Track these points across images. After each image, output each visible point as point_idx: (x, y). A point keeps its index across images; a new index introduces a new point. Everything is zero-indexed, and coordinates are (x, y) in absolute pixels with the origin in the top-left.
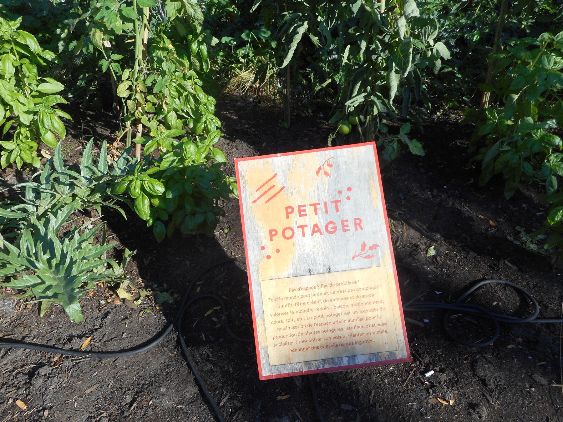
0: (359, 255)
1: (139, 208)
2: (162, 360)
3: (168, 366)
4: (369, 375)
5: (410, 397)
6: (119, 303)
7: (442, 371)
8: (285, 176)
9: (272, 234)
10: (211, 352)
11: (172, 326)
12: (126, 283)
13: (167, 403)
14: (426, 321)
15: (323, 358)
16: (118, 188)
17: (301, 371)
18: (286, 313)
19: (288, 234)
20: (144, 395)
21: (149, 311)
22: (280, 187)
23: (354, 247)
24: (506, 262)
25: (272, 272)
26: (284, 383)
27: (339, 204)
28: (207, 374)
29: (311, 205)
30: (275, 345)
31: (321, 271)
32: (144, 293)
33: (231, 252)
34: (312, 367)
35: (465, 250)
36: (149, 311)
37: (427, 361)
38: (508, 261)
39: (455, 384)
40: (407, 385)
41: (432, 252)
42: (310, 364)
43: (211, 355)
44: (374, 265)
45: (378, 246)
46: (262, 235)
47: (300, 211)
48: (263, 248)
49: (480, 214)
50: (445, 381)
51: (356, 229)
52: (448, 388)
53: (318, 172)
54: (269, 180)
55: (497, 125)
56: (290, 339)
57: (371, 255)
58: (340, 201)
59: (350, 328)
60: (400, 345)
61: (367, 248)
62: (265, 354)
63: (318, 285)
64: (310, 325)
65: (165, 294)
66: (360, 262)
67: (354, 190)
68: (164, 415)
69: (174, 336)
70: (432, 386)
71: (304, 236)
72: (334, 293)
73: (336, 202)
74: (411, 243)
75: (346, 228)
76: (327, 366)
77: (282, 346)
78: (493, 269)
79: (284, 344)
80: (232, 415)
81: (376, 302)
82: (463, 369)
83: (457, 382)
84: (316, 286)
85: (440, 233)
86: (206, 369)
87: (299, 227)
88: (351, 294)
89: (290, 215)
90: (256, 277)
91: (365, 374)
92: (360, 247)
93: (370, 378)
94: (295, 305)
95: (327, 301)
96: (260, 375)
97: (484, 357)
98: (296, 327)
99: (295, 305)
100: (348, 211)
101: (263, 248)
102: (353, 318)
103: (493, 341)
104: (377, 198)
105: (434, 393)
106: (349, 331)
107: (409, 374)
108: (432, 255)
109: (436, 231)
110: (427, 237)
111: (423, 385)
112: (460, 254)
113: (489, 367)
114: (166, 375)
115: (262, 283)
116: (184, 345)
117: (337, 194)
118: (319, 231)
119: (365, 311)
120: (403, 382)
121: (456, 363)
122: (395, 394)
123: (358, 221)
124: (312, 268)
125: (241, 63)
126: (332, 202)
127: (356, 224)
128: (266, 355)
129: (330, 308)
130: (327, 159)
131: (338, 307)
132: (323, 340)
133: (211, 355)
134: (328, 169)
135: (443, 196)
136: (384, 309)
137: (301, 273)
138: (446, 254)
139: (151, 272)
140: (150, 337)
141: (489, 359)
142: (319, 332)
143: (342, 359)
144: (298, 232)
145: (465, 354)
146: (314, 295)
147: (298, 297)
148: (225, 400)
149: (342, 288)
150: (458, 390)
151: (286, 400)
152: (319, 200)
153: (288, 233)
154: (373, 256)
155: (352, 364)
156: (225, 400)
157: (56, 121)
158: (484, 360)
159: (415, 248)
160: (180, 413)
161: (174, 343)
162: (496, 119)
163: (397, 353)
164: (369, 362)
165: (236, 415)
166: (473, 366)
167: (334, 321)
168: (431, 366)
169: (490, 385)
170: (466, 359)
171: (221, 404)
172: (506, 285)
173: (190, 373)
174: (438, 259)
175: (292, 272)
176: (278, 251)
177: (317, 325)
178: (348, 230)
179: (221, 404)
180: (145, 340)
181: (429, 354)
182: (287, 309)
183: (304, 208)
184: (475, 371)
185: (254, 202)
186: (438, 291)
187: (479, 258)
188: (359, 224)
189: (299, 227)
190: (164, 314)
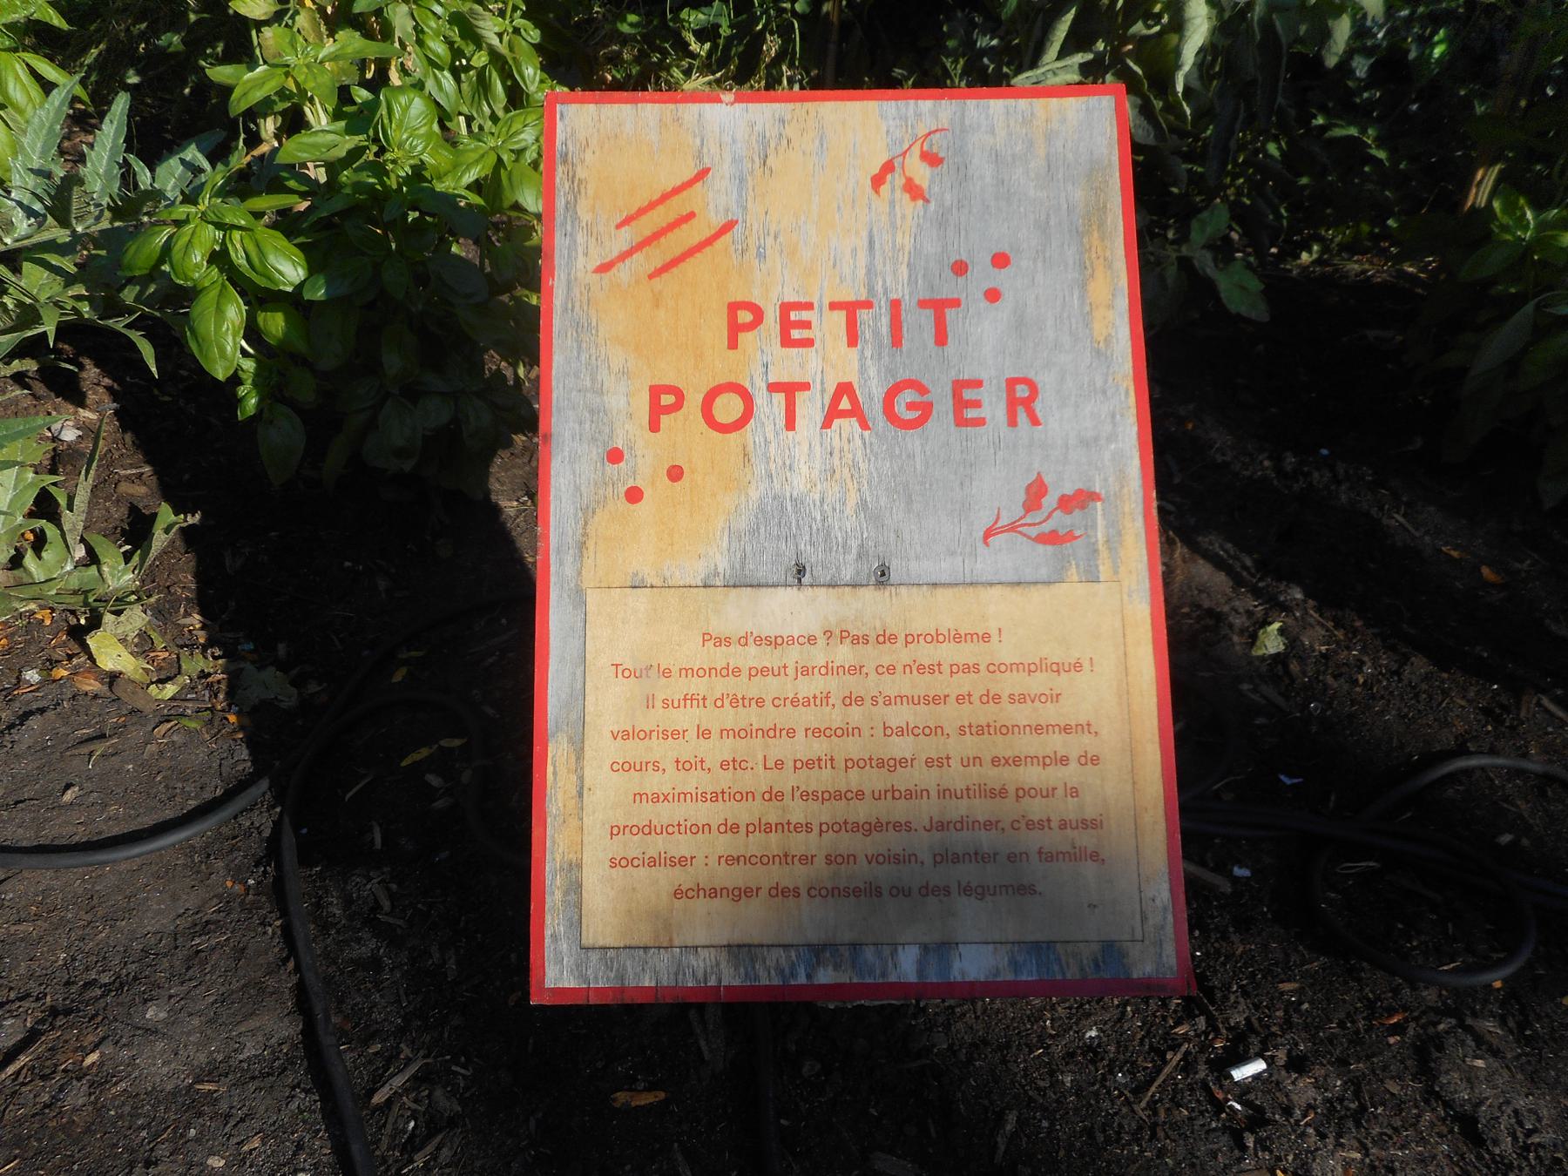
0: (1012, 528)
1: (201, 330)
2: (190, 901)
3: (205, 928)
4: (1000, 1048)
5: (1161, 1153)
6: (91, 685)
7: (1297, 1064)
8: (742, 180)
9: (662, 403)
10: (392, 896)
11: (264, 784)
12: (136, 619)
13: (159, 1066)
14: (1240, 872)
15: (813, 937)
16: (133, 248)
17: (712, 982)
18: (676, 734)
19: (727, 409)
20: (72, 1027)
21: (193, 725)
22: (717, 221)
23: (997, 492)
24: (1545, 701)
25: (641, 560)
26: (630, 1029)
27: (950, 314)
28: (353, 973)
29: (834, 306)
30: (614, 864)
31: (847, 574)
32: (195, 664)
33: (516, 527)
34: (762, 973)
35: (1393, 648)
36: (193, 725)
37: (1238, 1018)
38: (1557, 701)
39: (1350, 1124)
40: (1152, 1105)
41: (1271, 642)
42: (753, 960)
43: (386, 905)
44: (1073, 573)
45: (1095, 497)
46: (616, 401)
47: (786, 325)
48: (615, 456)
49: (1446, 544)
50: (1310, 1107)
51: (1012, 422)
52: (1323, 1136)
53: (877, 181)
54: (677, 191)
55: (1529, 249)
56: (682, 845)
57: (1062, 532)
58: (956, 303)
59: (942, 826)
60: (1153, 920)
61: (1050, 501)
62: (566, 893)
63: (828, 633)
64: (774, 796)
65: (271, 674)
66: (1010, 555)
67: (1021, 263)
68: (134, 1115)
69: (264, 821)
70: (1257, 1119)
71: (790, 424)
72: (891, 669)
73: (939, 307)
74: (1199, 607)
75: (971, 413)
76: (825, 976)
77: (643, 872)
78: (1498, 721)
79: (653, 862)
80: (411, 1146)
81: (1066, 729)
82: (1385, 1068)
83: (1359, 1116)
84: (819, 634)
85: (1301, 584)
86: (354, 955)
87: (773, 388)
88: (963, 683)
89: (743, 337)
90: (569, 571)
91: (985, 1042)
92: (1021, 497)
93: (1004, 1061)
94: (719, 703)
95: (860, 700)
96: (533, 981)
97: (1469, 1030)
98: (715, 797)
99: (719, 703)
100: (984, 344)
101: (615, 456)
102: (960, 785)
103: (1508, 971)
104: (1111, 306)
105: (1265, 1149)
106: (937, 835)
107: (1165, 1062)
108: (1272, 651)
109: (1293, 577)
110: (1256, 593)
111: (1217, 1113)
112: (1375, 660)
113: (1490, 1076)
114: (189, 959)
115: (592, 598)
116: (289, 856)
117: (948, 273)
118: (856, 412)
119: (1016, 761)
120: (1139, 1090)
121: (1356, 1040)
122: (1100, 1138)
123: (1022, 391)
124: (811, 556)
125: (693, 56)
126: (923, 304)
127: (1013, 404)
128: (572, 897)
129: (866, 732)
130: (922, 131)
131: (901, 732)
132: (820, 861)
133: (386, 905)
134: (921, 173)
135: (1316, 475)
136: (1095, 760)
137: (763, 573)
138: (1323, 656)
139: (239, 594)
140: (169, 814)
141: (1488, 1037)
142: (808, 828)
143: (894, 953)
144: (770, 408)
145: (1391, 1012)
146: (806, 671)
147: (737, 672)
148: (398, 1081)
149: (926, 653)
150: (1364, 1149)
151: (648, 1109)
152: (871, 289)
153: (727, 408)
154: (1070, 537)
155: (933, 978)
156: (398, 1081)
157: (17, 77)
158: (1470, 1042)
159: (1210, 622)
160: (200, 1114)
161: (256, 847)
162: (1526, 228)
163: (1135, 952)
164: (1010, 977)
165: (429, 1149)
166: (1425, 1058)
167: (880, 786)
168: (1255, 1041)
169: (1496, 1142)
170: (1398, 1029)
171: (378, 1098)
172: (1548, 779)
173: (285, 961)
174: (1294, 667)
175: (723, 565)
176: (675, 474)
177: (805, 796)
178: (980, 422)
179: (378, 1098)
180: (148, 821)
181: (1246, 994)
182: (686, 718)
183: (805, 315)
184: (1435, 1078)
185: (604, 268)
186: (1291, 776)
187: (1443, 682)
188: (1028, 403)
189: (773, 388)
190: (250, 743)
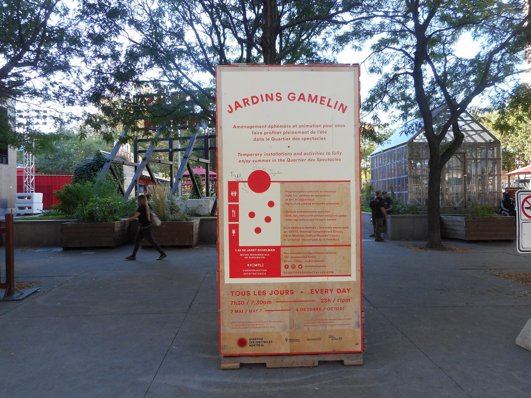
71: (330, 99)
75: (322, 102)
118: (304, 99)
188: (247, 102)
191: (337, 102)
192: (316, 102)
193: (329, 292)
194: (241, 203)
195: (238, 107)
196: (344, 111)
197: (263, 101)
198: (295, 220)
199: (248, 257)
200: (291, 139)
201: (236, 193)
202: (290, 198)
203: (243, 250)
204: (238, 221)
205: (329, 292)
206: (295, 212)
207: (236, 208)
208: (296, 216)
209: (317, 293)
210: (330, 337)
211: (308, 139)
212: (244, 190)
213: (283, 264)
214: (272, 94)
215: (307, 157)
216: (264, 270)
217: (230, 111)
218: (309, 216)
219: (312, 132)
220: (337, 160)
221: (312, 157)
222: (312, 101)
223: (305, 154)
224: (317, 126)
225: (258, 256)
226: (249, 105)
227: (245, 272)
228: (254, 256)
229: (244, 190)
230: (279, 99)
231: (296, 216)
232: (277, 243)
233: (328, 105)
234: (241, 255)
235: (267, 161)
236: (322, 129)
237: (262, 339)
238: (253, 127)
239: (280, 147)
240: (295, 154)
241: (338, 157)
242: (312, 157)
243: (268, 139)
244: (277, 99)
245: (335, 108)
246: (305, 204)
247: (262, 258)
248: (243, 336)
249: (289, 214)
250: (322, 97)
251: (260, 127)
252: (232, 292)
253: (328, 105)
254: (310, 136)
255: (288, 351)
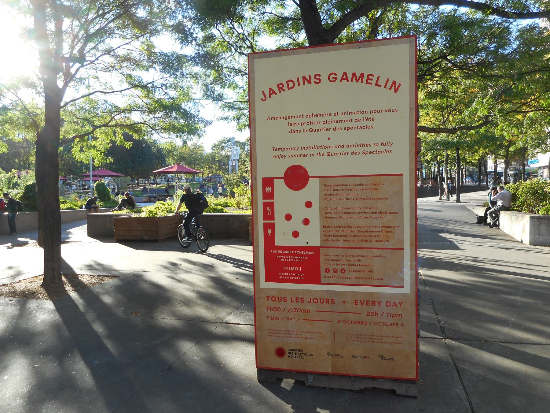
71: (378, 77)
75: (369, 81)
188: (282, 88)
191: (388, 80)
192: (362, 82)
193: (377, 304)
194: (277, 200)
195: (272, 94)
196: (396, 91)
197: (299, 85)
198: (336, 218)
199: (286, 258)
200: (332, 130)
201: (270, 189)
202: (329, 193)
203: (279, 251)
204: (274, 220)
205: (377, 304)
206: (335, 209)
207: (272, 205)
208: (337, 213)
209: (362, 304)
210: (379, 356)
211: (352, 128)
212: (280, 186)
213: (323, 268)
214: (310, 76)
215: (350, 150)
216: (301, 275)
217: (264, 99)
218: (353, 213)
219: (356, 120)
220: (387, 152)
221: (356, 149)
222: (357, 81)
223: (348, 146)
224: (363, 113)
225: (295, 259)
226: (284, 90)
227: (281, 276)
228: (291, 258)
229: (280, 186)
230: (318, 81)
231: (337, 213)
232: (318, 245)
233: (376, 85)
234: (277, 256)
235: (304, 155)
236: (368, 115)
237: (302, 351)
238: (289, 117)
239: (320, 139)
240: (336, 147)
241: (388, 148)
242: (356, 149)
243: (306, 131)
244: (315, 82)
245: (385, 87)
246: (347, 199)
247: (299, 261)
248: (281, 345)
249: (329, 211)
250: (369, 75)
251: (297, 117)
252: (268, 297)
253: (376, 85)
254: (354, 124)
255: (330, 371)
